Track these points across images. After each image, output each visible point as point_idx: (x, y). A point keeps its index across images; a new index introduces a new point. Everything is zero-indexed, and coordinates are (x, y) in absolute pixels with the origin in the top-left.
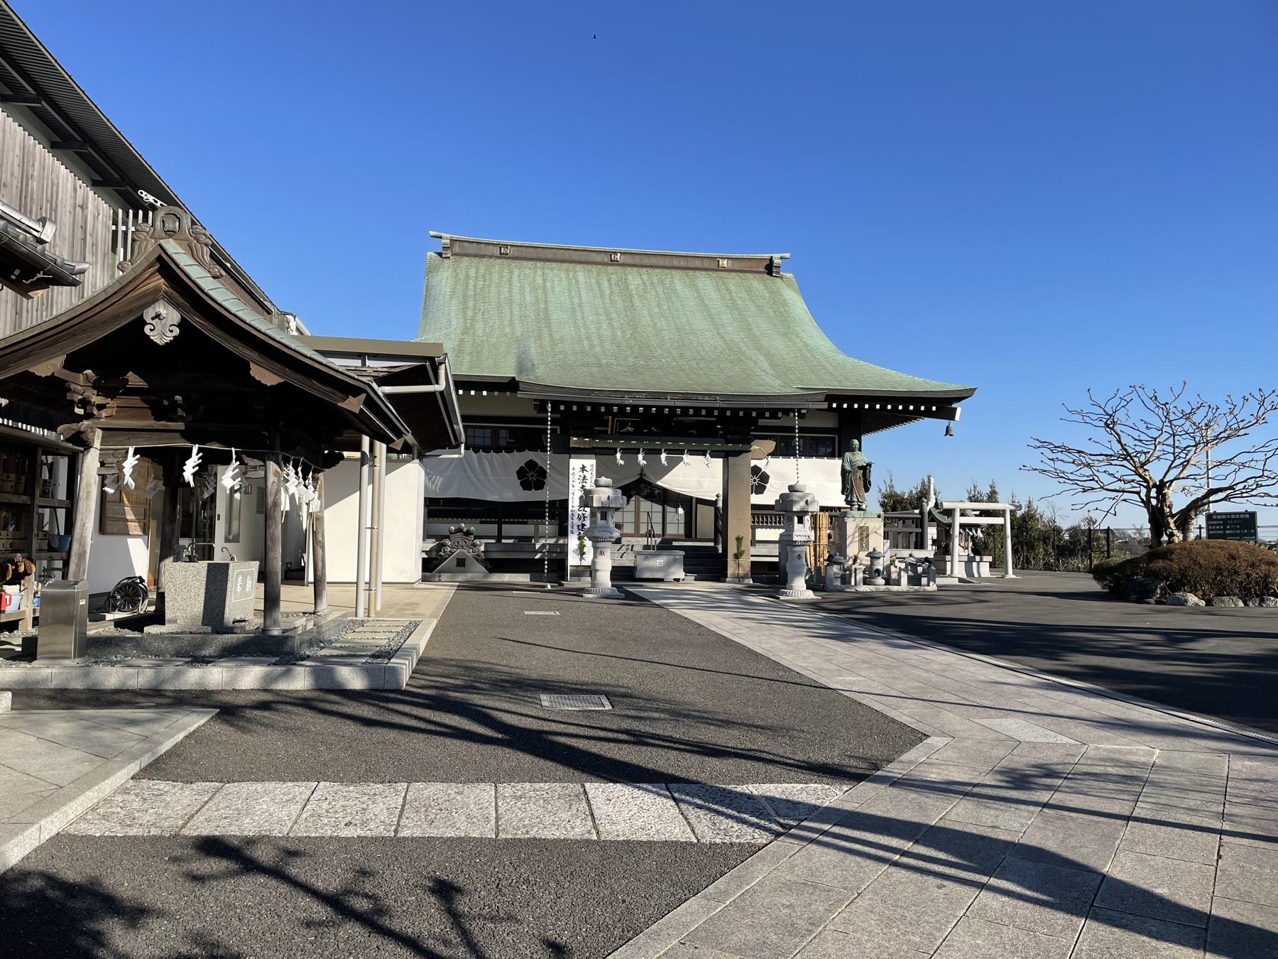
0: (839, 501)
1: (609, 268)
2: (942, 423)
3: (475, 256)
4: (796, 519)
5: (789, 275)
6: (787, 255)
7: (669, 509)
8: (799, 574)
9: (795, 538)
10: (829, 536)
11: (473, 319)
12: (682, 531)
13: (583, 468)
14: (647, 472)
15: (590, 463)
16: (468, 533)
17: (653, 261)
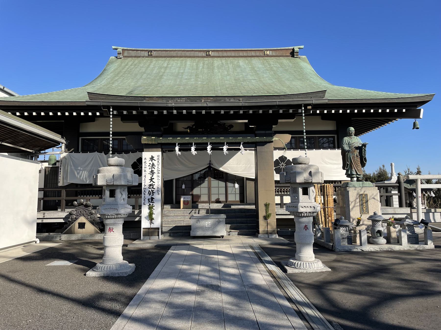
0: (341, 175)
1: (205, 59)
2: (410, 121)
3: (135, 57)
4: (300, 190)
5: (303, 57)
6: (302, 47)
7: (229, 185)
8: (305, 244)
9: (301, 210)
10: (335, 201)
11: (116, 80)
12: (238, 199)
13: (152, 158)
14: (213, 162)
15: (157, 154)
16: (87, 206)
17: (229, 54)
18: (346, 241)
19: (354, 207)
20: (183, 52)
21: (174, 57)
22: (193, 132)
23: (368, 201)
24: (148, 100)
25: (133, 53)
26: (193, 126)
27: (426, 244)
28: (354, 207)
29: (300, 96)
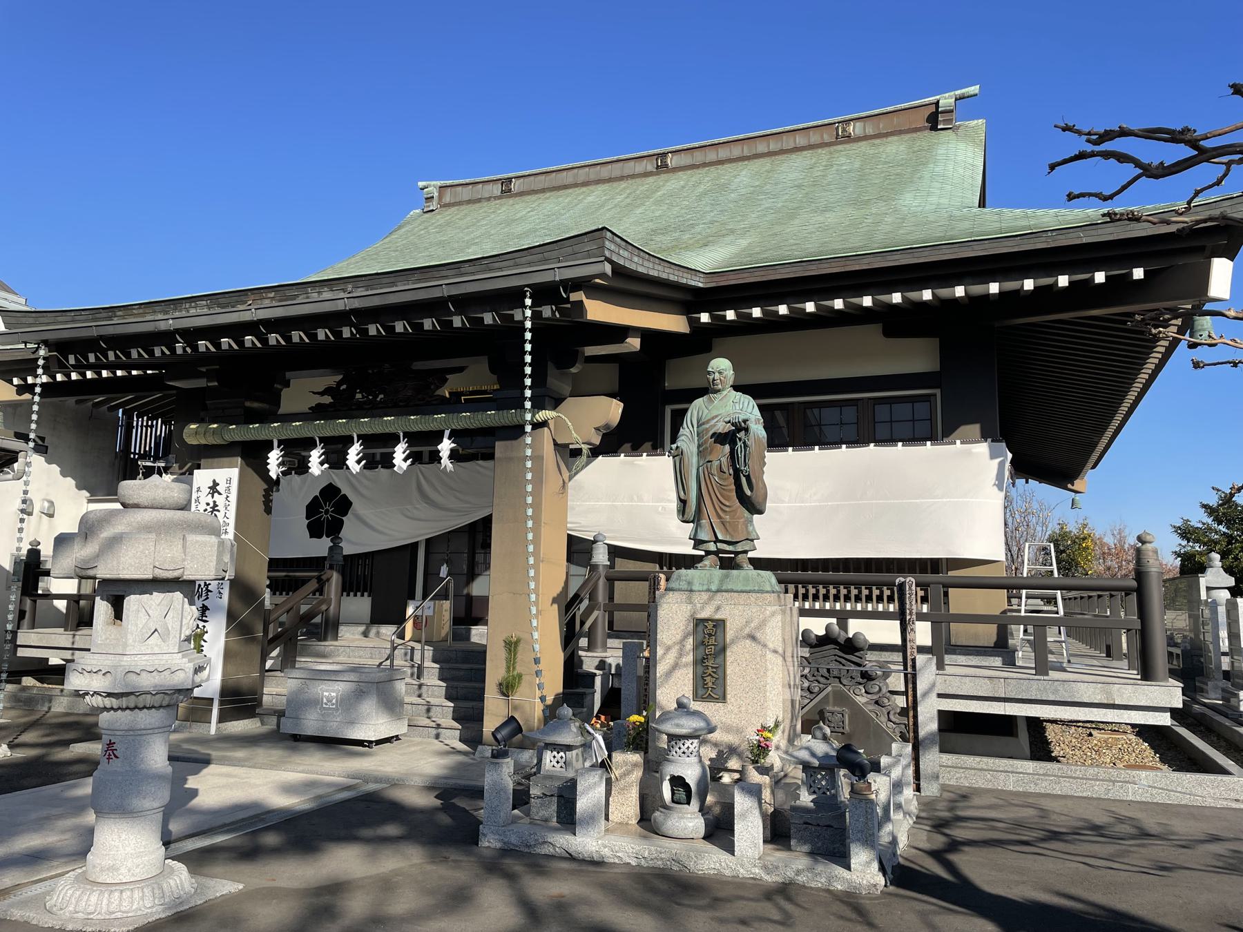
3: (469, 202)
6: (974, 89)
13: (214, 489)
18: (555, 807)
19: (675, 666)
20: (592, 170)
21: (566, 187)
22: (339, 404)
23: (724, 649)
24: (123, 317)
25: (465, 193)
26: (339, 383)
27: (843, 859)
28: (675, 666)
29: (523, 260)
